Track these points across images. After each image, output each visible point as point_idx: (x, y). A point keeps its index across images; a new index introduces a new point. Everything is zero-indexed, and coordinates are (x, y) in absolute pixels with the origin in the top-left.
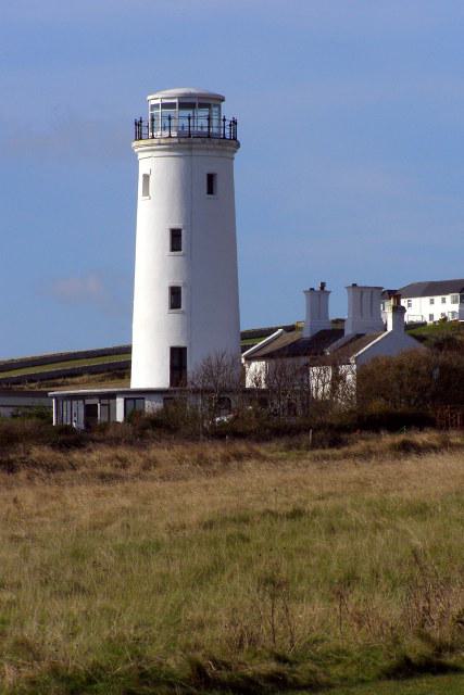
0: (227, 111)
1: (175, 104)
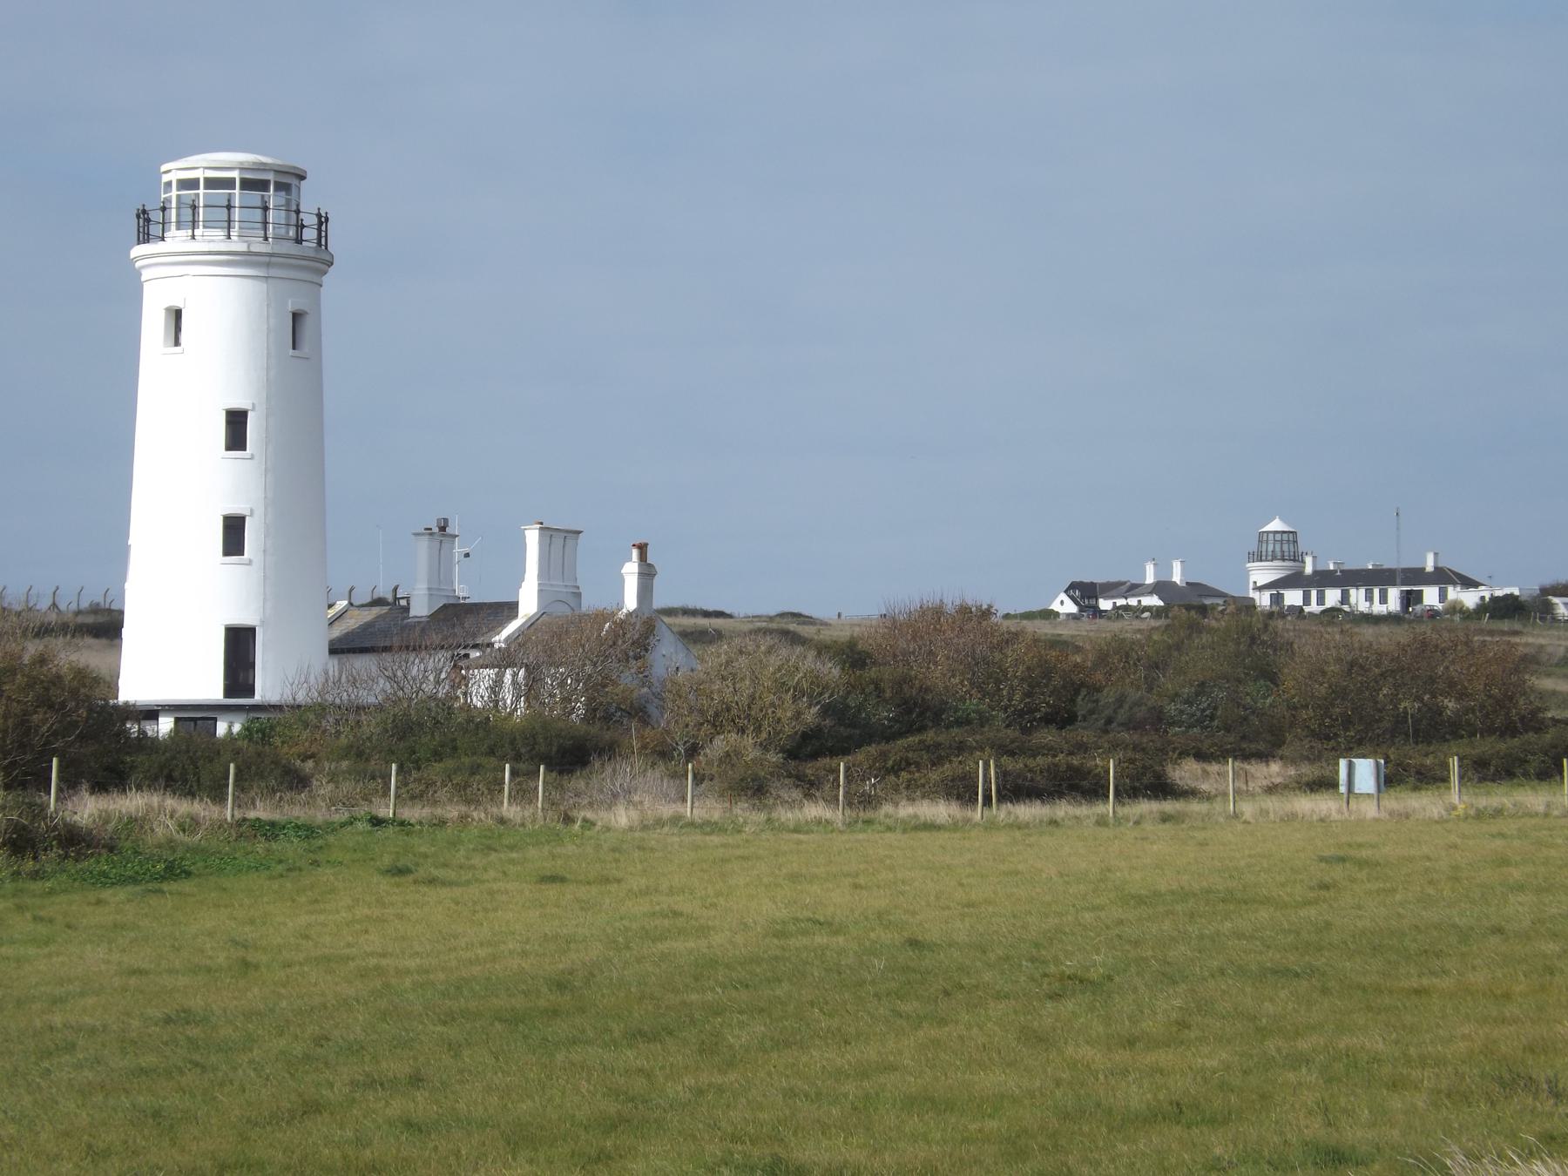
0: (310, 200)
1: (197, 180)
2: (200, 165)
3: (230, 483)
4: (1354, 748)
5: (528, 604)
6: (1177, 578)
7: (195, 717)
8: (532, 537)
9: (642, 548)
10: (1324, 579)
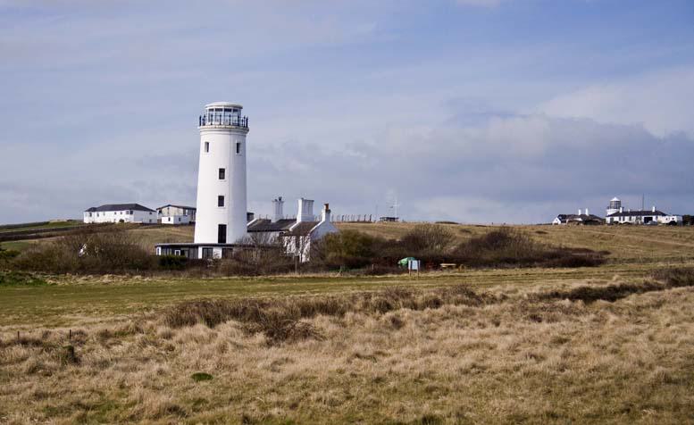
0: (244, 113)
2: (214, 105)
3: (223, 188)
4: (201, 260)
5: (299, 220)
6: (587, 214)
7: (208, 248)
8: (300, 202)
9: (327, 205)
10: (625, 214)
